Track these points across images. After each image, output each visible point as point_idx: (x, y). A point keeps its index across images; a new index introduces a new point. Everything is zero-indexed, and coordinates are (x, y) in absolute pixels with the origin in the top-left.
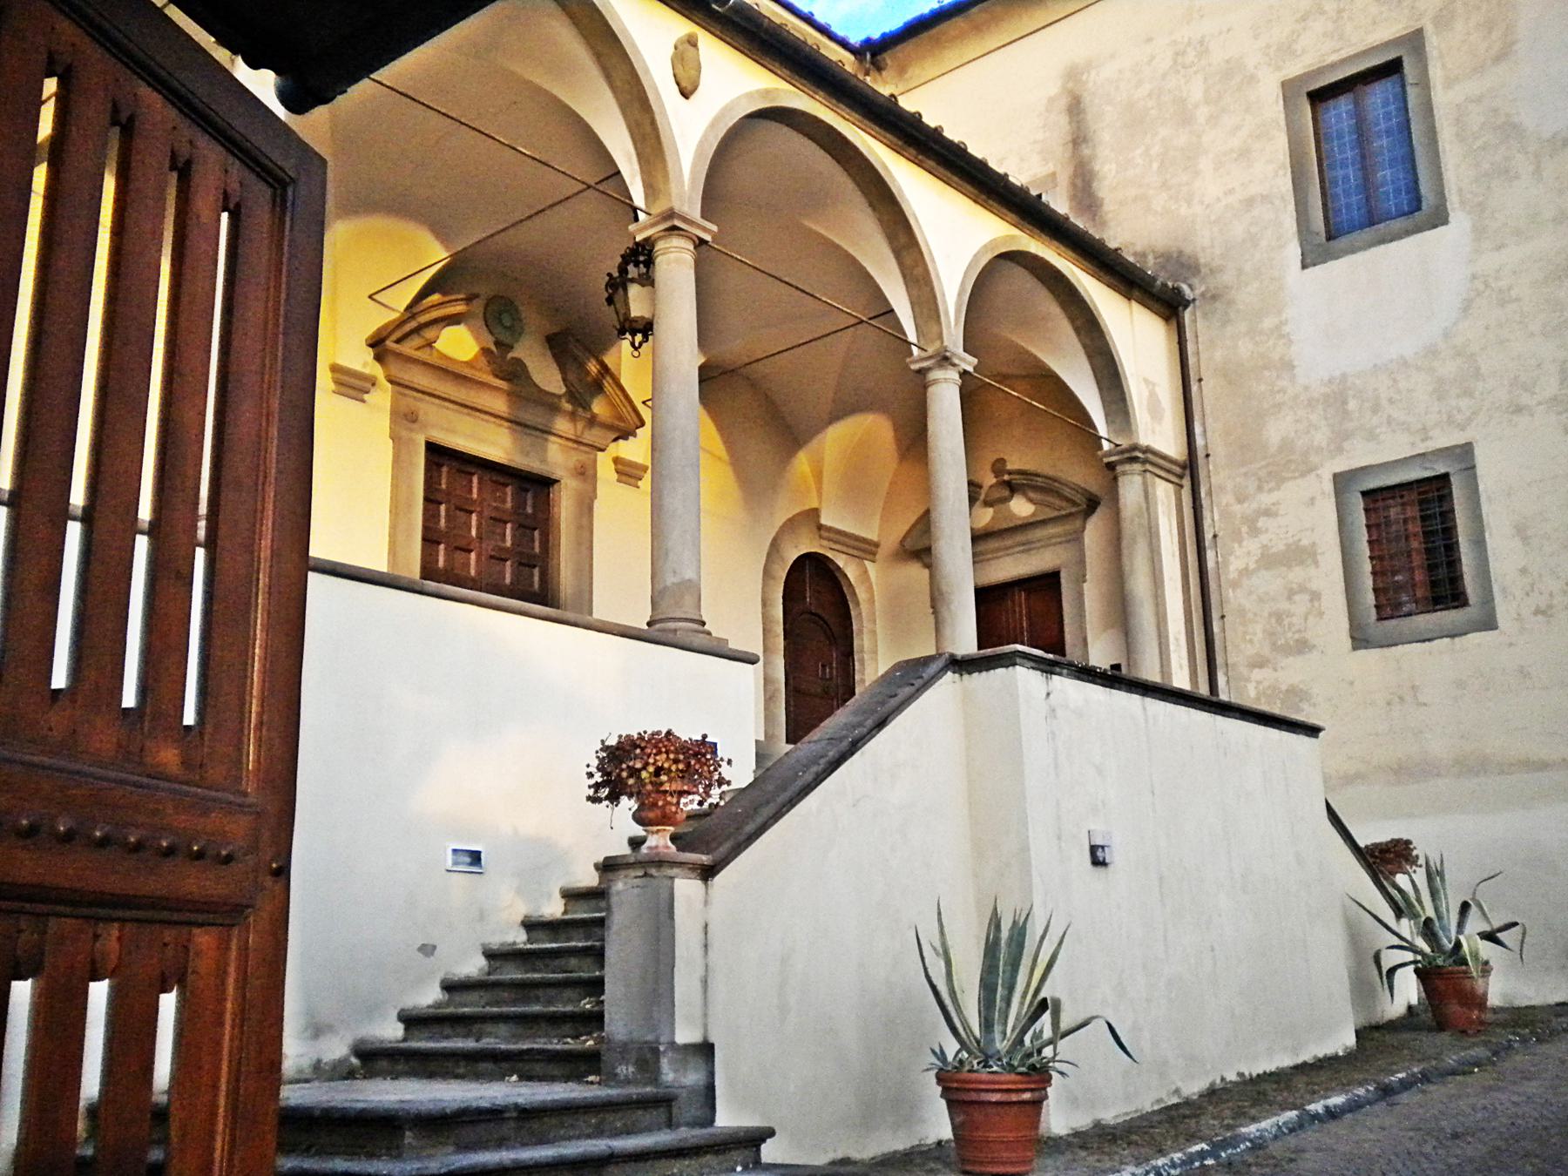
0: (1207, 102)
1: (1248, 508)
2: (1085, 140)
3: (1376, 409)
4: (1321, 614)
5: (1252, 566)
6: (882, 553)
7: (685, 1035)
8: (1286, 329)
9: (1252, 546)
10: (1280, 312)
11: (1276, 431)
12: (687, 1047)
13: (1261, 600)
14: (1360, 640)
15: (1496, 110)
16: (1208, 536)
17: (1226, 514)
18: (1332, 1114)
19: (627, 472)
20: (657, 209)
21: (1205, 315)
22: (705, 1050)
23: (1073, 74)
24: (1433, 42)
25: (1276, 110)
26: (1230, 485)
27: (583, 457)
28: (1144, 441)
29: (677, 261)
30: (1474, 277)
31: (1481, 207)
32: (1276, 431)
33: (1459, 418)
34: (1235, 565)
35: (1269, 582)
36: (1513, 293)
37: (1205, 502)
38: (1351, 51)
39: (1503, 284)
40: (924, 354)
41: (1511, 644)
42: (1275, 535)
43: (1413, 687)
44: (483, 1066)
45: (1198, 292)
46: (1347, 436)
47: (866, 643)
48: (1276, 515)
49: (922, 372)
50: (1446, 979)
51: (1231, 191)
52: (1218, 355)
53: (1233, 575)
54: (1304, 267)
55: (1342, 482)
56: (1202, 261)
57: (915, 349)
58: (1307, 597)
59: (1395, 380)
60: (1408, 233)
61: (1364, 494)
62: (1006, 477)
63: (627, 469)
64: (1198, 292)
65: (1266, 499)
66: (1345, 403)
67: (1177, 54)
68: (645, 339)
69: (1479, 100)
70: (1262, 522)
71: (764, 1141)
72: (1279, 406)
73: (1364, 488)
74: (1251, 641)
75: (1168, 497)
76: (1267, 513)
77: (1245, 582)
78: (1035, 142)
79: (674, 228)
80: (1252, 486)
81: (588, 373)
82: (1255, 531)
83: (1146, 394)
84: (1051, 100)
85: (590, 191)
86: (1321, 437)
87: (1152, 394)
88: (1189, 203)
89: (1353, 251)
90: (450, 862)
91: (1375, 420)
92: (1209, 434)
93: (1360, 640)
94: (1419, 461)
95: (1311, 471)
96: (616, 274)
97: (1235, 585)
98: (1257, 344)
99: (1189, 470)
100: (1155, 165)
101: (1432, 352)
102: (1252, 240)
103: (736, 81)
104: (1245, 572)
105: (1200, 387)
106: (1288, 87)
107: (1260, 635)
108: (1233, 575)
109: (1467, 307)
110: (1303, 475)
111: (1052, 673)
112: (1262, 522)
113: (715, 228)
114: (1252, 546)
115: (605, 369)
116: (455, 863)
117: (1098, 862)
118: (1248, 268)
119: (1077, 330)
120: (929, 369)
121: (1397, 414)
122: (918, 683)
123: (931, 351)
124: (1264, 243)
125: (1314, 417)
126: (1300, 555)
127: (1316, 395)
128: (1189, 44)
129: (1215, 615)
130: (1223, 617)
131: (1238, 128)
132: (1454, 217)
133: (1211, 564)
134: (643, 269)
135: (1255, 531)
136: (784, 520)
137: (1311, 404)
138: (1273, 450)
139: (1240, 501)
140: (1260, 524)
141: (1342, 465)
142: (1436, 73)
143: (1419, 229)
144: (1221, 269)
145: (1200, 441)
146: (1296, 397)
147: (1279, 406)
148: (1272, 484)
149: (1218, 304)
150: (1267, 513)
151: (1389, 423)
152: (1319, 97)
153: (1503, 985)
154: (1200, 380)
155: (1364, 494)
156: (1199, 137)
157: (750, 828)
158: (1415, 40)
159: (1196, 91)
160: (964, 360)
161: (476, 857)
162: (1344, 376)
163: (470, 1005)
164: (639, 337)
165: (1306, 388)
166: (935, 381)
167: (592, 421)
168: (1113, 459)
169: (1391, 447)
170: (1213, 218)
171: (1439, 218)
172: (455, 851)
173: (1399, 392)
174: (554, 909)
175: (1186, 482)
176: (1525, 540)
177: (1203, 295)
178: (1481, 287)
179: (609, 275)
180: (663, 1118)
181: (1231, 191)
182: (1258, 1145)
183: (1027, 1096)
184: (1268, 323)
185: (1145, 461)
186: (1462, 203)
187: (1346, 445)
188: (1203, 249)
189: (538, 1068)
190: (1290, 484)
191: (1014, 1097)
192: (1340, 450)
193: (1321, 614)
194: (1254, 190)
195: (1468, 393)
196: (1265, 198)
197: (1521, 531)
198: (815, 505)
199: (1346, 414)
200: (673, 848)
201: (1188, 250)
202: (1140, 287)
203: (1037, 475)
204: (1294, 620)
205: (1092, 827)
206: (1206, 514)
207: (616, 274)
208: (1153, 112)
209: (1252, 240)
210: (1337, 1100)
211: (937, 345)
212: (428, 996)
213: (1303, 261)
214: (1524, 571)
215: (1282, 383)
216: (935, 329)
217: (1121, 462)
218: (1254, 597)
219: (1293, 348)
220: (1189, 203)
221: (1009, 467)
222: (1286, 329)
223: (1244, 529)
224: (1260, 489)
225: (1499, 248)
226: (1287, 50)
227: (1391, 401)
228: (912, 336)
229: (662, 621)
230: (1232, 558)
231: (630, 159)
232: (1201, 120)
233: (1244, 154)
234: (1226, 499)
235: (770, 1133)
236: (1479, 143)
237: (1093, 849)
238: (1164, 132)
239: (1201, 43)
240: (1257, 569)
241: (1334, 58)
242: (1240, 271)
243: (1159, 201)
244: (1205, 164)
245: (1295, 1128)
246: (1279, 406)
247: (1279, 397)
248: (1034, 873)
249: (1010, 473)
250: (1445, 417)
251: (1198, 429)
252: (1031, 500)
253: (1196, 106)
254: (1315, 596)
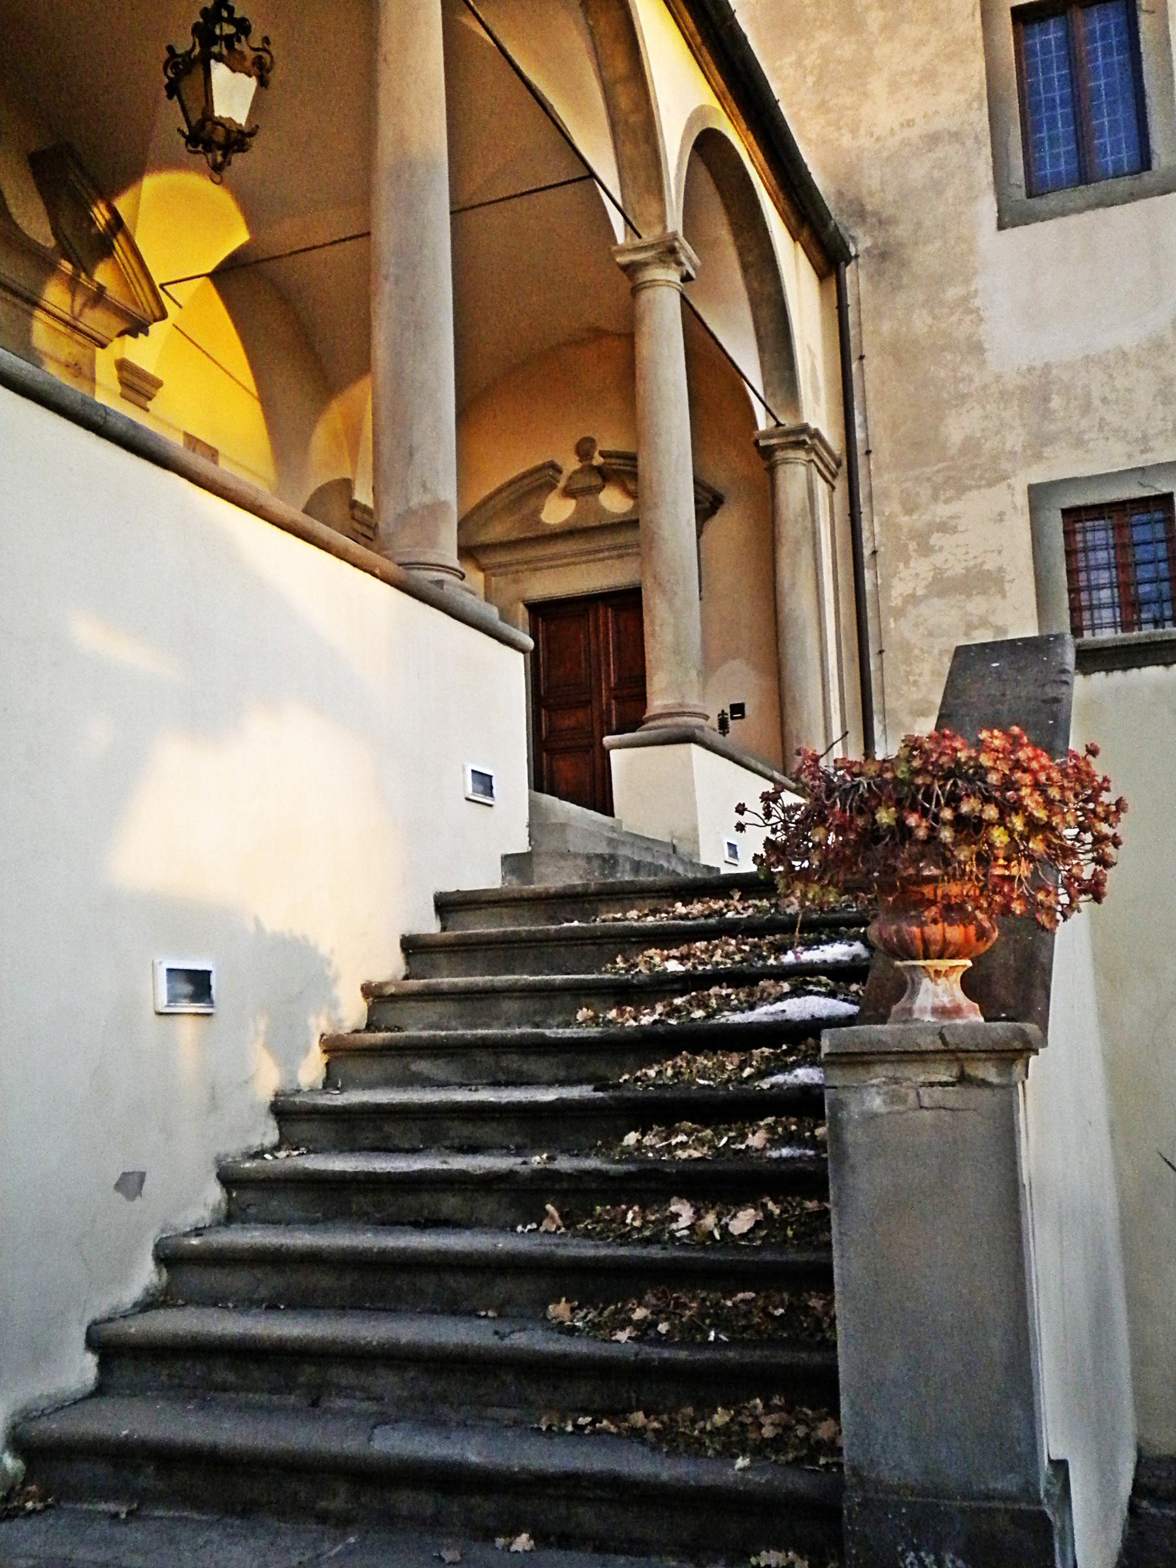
1: (919, 520)
5: (920, 592)
8: (977, 302)
9: (922, 567)
10: (967, 281)
11: (957, 429)
13: (931, 634)
16: (867, 552)
17: (890, 525)
21: (870, 277)
26: (895, 490)
27: (76, 349)
32: (957, 429)
34: (899, 590)
37: (864, 509)
42: (953, 556)
44: (405, 1501)
46: (1046, 440)
48: (954, 530)
49: (631, 269)
52: (886, 327)
53: (896, 601)
54: (1001, 226)
55: (1038, 494)
59: (1111, 376)
61: (1066, 513)
63: (136, 381)
65: (942, 511)
66: (1046, 400)
70: (935, 539)
72: (963, 398)
74: (915, 683)
76: (944, 527)
80: (925, 492)
81: (92, 222)
82: (926, 550)
86: (1015, 439)
88: (854, 132)
89: (1064, 213)
90: (163, 997)
91: (1084, 424)
92: (871, 424)
94: (1139, 474)
95: (1004, 479)
97: (899, 613)
99: (847, 467)
100: (810, 80)
102: (937, 187)
104: (912, 599)
105: (861, 369)
107: (927, 677)
108: (896, 601)
110: (990, 485)
112: (935, 539)
114: (922, 567)
115: (116, 223)
116: (173, 998)
118: (928, 223)
120: (644, 264)
121: (1113, 418)
123: (648, 237)
124: (950, 193)
125: (1007, 415)
127: (1010, 387)
129: (872, 650)
130: (881, 652)
131: (921, 43)
133: (868, 586)
135: (926, 550)
138: (953, 451)
139: (909, 512)
140: (932, 542)
141: (1039, 475)
143: (1147, 194)
144: (892, 221)
145: (859, 434)
146: (985, 387)
148: (950, 493)
150: (944, 527)
151: (1101, 429)
154: (861, 358)
155: (1066, 513)
156: (870, 49)
161: (198, 984)
162: (1047, 366)
165: (998, 378)
166: (653, 283)
167: (98, 297)
168: (773, 441)
170: (885, 154)
173: (1114, 390)
175: (841, 484)
181: (910, 123)
184: (952, 293)
185: (813, 449)
187: (1048, 451)
188: (871, 194)
189: (587, 1517)
190: (974, 494)
192: (1039, 457)
194: (941, 123)
196: (956, 136)
198: (348, 476)
199: (1048, 416)
202: (812, 225)
206: (865, 525)
209: (937, 187)
211: (657, 231)
213: (999, 219)
215: (965, 370)
216: (654, 208)
217: (783, 447)
218: (921, 630)
219: (983, 327)
220: (854, 132)
222: (977, 302)
223: (912, 546)
224: (935, 498)
227: (1104, 400)
233: (928, 77)
234: (891, 507)
238: (824, 38)
242: (919, 225)
244: (877, 84)
251: (858, 419)
253: (868, 8)
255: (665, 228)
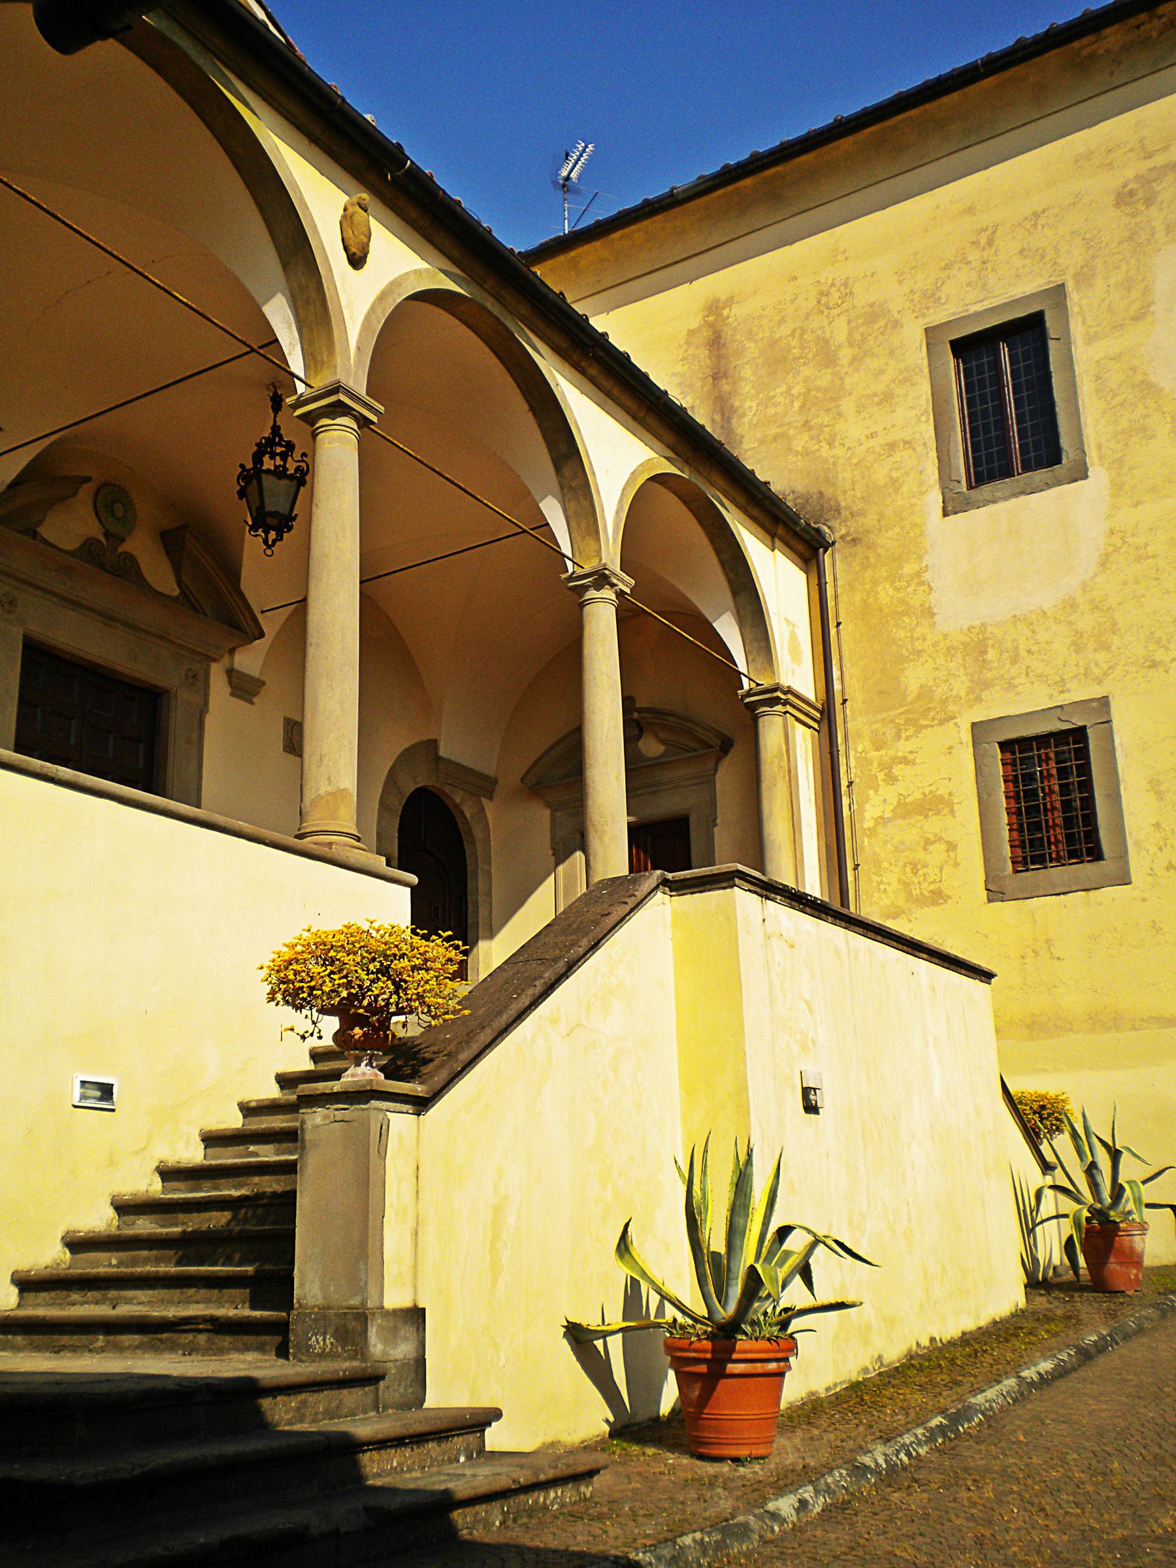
0: (851, 345)
2: (725, 375)
3: (1015, 660)
4: (956, 865)
6: (500, 791)
7: (395, 1298)
8: (927, 576)
10: (920, 558)
11: (914, 678)
12: (396, 1313)
13: (896, 849)
14: (995, 893)
15: (1134, 369)
16: (844, 783)
17: (864, 762)
18: (1045, 1381)
19: (245, 688)
20: (320, 382)
22: (416, 1316)
23: (714, 308)
24: (1074, 298)
25: (919, 357)
28: (785, 682)
29: (340, 440)
30: (1112, 532)
31: (1120, 462)
32: (914, 678)
33: (1096, 671)
35: (908, 832)
36: (1150, 550)
38: (995, 302)
39: (1141, 540)
40: (579, 571)
41: (1144, 900)
42: (913, 783)
43: (1047, 941)
44: (127, 1339)
45: (837, 535)
46: (986, 685)
47: (481, 886)
50: (1101, 1235)
51: (873, 435)
56: (843, 504)
57: (569, 564)
58: (944, 846)
60: (1048, 486)
61: (1004, 746)
62: (636, 715)
64: (837, 535)
65: (903, 747)
66: (985, 652)
67: (822, 294)
68: (280, 537)
69: (1117, 358)
70: (897, 770)
71: (490, 1424)
73: (1002, 738)
75: (805, 739)
76: (905, 761)
77: (880, 829)
78: (673, 374)
79: (340, 403)
82: (892, 779)
83: (787, 636)
84: (691, 333)
85: (254, 354)
86: (960, 686)
87: (793, 636)
88: (831, 444)
91: (1014, 671)
92: (846, 678)
93: (995, 893)
96: (249, 465)
98: (897, 589)
99: (825, 717)
100: (797, 405)
101: (1071, 605)
103: (398, 263)
104: (881, 821)
106: (930, 333)
109: (1105, 562)
110: (941, 723)
111: (767, 898)
113: (382, 409)
114: (889, 793)
116: (83, 1097)
117: (811, 1108)
119: (723, 564)
122: (632, 902)
123: (588, 568)
124: (905, 489)
126: (934, 804)
128: (833, 285)
131: (881, 372)
132: (1096, 471)
134: (279, 462)
136: (401, 750)
137: (950, 651)
142: (1077, 329)
143: (1059, 483)
145: (837, 686)
147: (919, 653)
149: (859, 549)
151: (1027, 674)
152: (960, 347)
153: (1159, 1243)
154: (839, 624)
155: (1004, 746)
157: (465, 1056)
158: (1058, 292)
159: (839, 332)
160: (623, 581)
161: (106, 1091)
163: (107, 1263)
164: (273, 535)
165: (946, 636)
169: (1030, 698)
171: (1080, 473)
172: (83, 1083)
174: (194, 1154)
176: (1159, 795)
177: (842, 537)
178: (1119, 543)
179: (242, 466)
180: (370, 1399)
181: (873, 435)
182: (992, 1418)
183: (773, 1366)
184: (908, 569)
186: (1101, 458)
187: (985, 695)
191: (759, 1367)
192: (978, 699)
193: (956, 865)
195: (1106, 647)
197: (1155, 786)
200: (382, 1076)
201: (828, 492)
203: (671, 714)
204: (929, 870)
205: (803, 1069)
207: (249, 465)
208: (795, 351)
210: (1046, 1366)
212: (49, 1254)
213: (944, 508)
214: (1157, 825)
215: (920, 631)
216: (593, 545)
218: (890, 847)
220: (831, 444)
221: (638, 705)
222: (927, 576)
225: (1136, 505)
226: (932, 297)
227: (1029, 652)
228: (566, 549)
229: (312, 834)
230: (867, 807)
231: (290, 327)
232: (845, 362)
233: (887, 398)
235: (496, 1414)
236: (1119, 399)
237: (806, 1092)
238: (806, 372)
239: (846, 285)
240: (893, 819)
241: (978, 308)
243: (801, 442)
244: (848, 405)
245: (1020, 1398)
246: (919, 653)
247: (918, 645)
248: (752, 1116)
249: (640, 711)
250: (1082, 671)
252: (662, 741)
253: (840, 347)
254: (952, 847)
255: (601, 559)
